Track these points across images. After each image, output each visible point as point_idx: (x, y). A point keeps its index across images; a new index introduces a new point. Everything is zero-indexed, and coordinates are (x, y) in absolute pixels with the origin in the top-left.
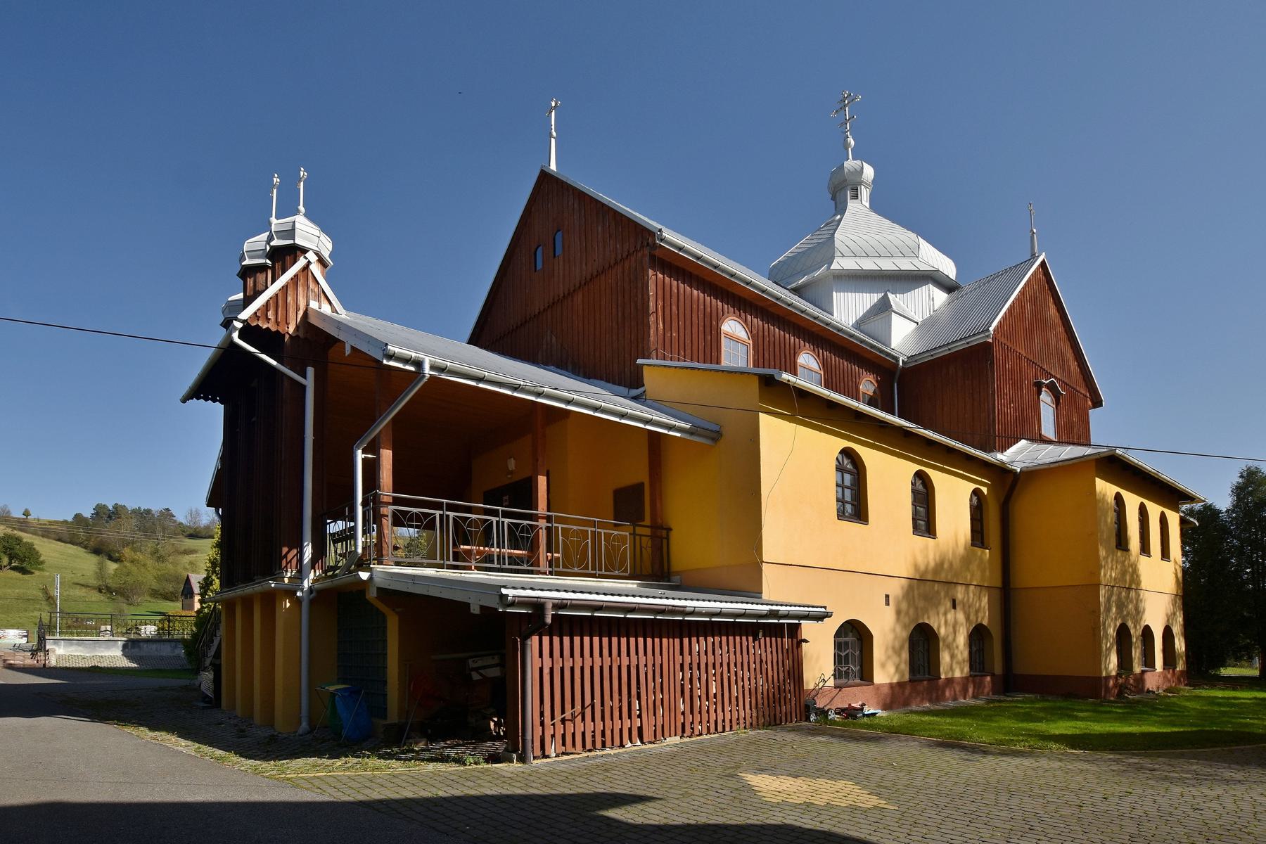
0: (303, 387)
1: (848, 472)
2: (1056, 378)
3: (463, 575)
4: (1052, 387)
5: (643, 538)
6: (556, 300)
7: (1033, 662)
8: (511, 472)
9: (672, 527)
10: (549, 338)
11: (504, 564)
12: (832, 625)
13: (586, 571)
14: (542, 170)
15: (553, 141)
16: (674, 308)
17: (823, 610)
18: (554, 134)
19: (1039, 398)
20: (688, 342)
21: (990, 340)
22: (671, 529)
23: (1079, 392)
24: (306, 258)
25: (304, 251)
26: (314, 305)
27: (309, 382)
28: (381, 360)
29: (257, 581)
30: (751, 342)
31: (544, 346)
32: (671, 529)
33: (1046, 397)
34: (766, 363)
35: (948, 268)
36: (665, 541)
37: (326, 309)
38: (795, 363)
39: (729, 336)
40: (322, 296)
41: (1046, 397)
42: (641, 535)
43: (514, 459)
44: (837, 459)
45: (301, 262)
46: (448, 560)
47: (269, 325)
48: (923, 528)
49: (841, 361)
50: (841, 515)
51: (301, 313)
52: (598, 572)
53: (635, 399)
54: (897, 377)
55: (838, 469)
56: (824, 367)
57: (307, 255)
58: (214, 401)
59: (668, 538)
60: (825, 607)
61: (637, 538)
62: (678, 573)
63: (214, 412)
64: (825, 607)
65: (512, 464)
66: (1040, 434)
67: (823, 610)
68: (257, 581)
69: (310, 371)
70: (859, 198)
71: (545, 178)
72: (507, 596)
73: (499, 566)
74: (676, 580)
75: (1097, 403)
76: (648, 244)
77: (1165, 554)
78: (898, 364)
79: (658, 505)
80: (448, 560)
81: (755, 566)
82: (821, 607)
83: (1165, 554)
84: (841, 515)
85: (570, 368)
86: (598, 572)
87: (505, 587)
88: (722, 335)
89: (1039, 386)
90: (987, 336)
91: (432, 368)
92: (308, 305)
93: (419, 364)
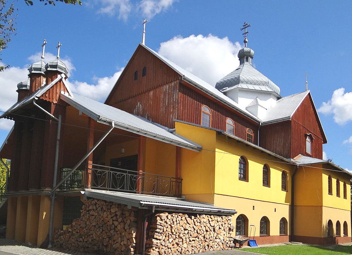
0: (58, 121)
1: (242, 164)
2: (312, 133)
3: (115, 193)
4: (310, 137)
5: (173, 182)
6: (142, 92)
7: (299, 232)
8: (122, 153)
9: (183, 179)
10: (139, 105)
11: (128, 190)
12: (236, 216)
13: (154, 193)
14: (140, 44)
15: (144, 34)
16: (186, 101)
17: (234, 211)
18: (144, 31)
19: (306, 140)
20: (191, 114)
21: (291, 120)
22: (182, 180)
23: (319, 138)
24: (61, 76)
25: (60, 73)
26: (62, 92)
27: (60, 120)
28: (96, 120)
29: (30, 191)
30: (211, 114)
31: (137, 108)
32: (182, 180)
33: (308, 139)
34: (219, 128)
35: (278, 89)
36: (180, 183)
37: (66, 95)
38: (225, 122)
39: (204, 112)
40: (66, 90)
41: (308, 139)
42: (172, 181)
43: (124, 149)
44: (240, 159)
45: (59, 77)
46: (110, 188)
47: (46, 99)
48: (266, 183)
49: (243, 126)
50: (240, 179)
51: (58, 95)
52: (158, 194)
53: (171, 132)
54: (259, 128)
55: (240, 163)
56: (235, 124)
57: (62, 75)
58: (11, 119)
59: (181, 182)
60: (235, 210)
61: (171, 182)
62: (184, 195)
63: (9, 124)
64: (235, 210)
65: (123, 150)
66: (306, 152)
67: (234, 211)
68: (30, 191)
69: (60, 117)
70: (249, 61)
71: (140, 47)
72: (142, 204)
73: (126, 190)
74: (184, 197)
75: (325, 142)
76: (179, 79)
77: (345, 197)
78: (260, 124)
79: (179, 171)
80: (110, 188)
81: (212, 194)
82: (234, 210)
83: (345, 197)
84: (240, 179)
85: (146, 118)
86: (158, 194)
87: (141, 201)
88: (202, 112)
89: (306, 136)
90: (289, 118)
91: (115, 124)
92: (60, 93)
93: (111, 123)
